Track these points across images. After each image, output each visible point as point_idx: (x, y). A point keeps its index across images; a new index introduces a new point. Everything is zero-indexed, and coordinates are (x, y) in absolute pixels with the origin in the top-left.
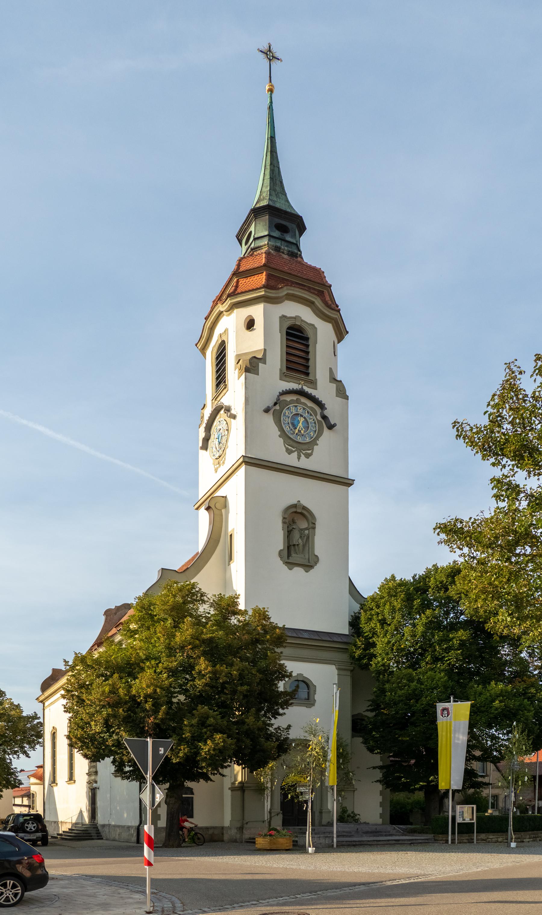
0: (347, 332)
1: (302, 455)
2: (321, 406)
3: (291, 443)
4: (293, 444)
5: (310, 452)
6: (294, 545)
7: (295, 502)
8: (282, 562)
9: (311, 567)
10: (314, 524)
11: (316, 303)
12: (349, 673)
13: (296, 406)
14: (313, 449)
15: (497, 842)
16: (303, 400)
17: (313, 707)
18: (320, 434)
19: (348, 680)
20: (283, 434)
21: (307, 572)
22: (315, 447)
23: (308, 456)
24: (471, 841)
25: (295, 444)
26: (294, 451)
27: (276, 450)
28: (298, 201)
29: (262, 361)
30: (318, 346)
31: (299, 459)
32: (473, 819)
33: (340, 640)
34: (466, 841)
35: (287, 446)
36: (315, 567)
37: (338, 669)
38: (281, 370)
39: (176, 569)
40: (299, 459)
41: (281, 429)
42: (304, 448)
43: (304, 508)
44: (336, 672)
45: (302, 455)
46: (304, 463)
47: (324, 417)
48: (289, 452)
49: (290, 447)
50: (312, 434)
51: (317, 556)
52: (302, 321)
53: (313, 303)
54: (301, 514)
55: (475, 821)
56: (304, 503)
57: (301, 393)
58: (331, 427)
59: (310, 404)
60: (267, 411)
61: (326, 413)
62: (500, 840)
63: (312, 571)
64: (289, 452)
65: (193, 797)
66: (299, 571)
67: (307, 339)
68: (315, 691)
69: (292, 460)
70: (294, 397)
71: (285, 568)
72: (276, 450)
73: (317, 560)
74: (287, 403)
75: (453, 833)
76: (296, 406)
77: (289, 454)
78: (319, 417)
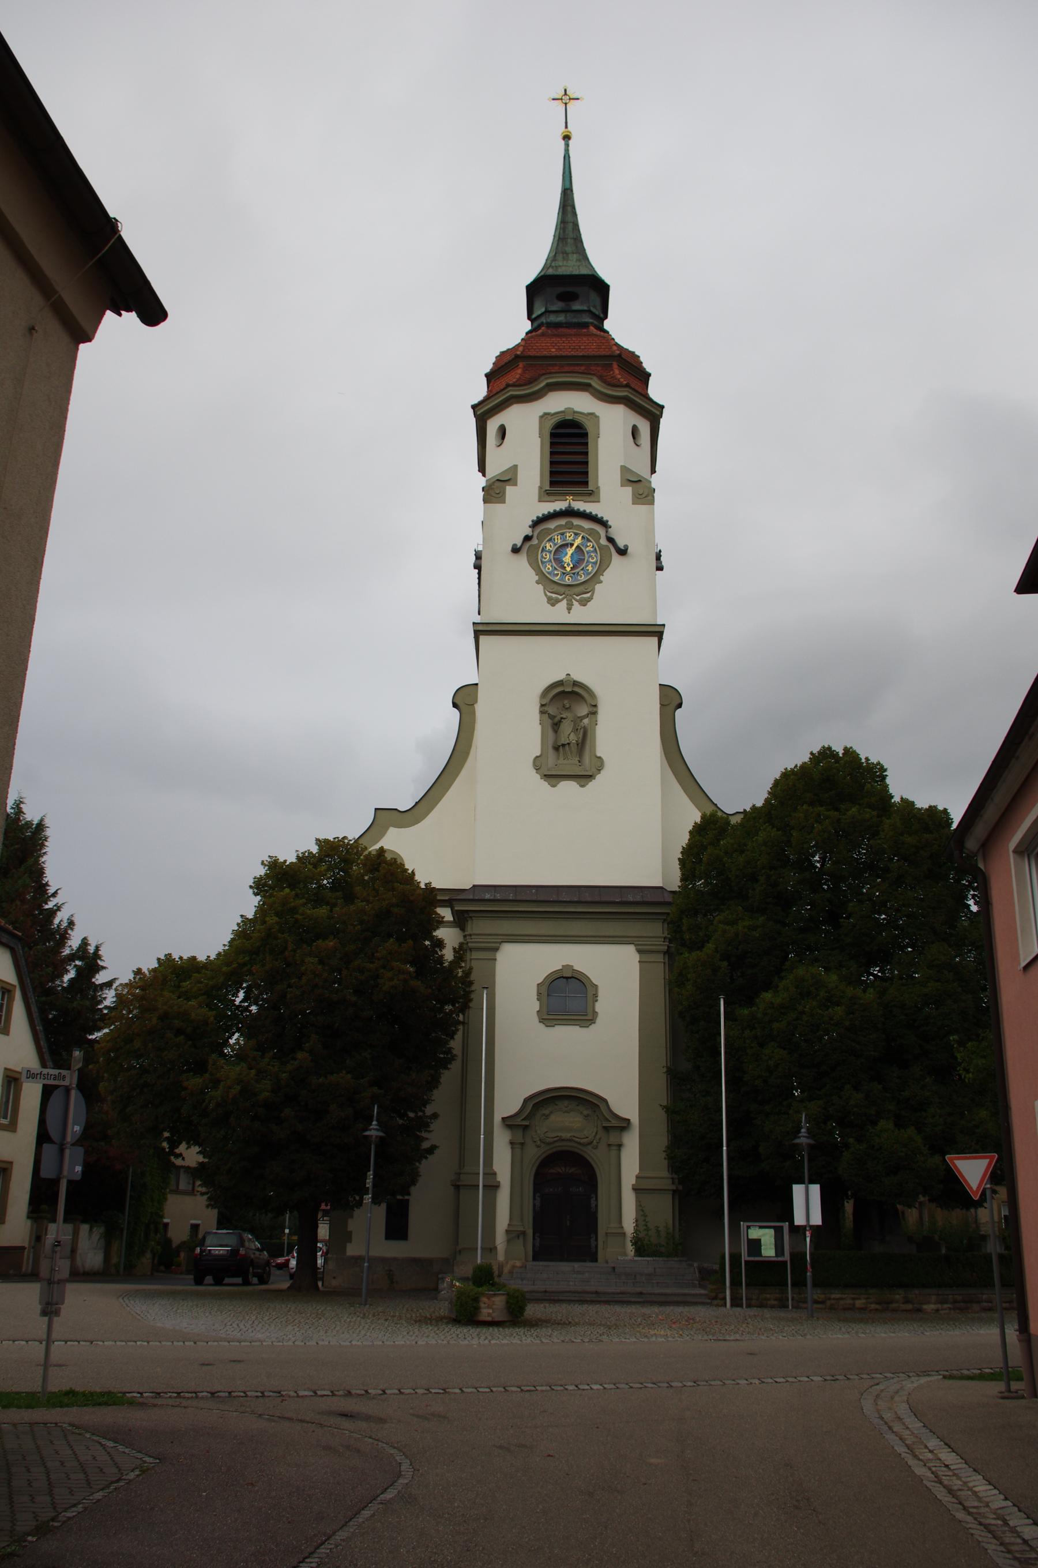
0: (662, 407)
1: (575, 602)
2: (604, 524)
3: (556, 588)
4: (559, 590)
5: (588, 595)
6: (563, 745)
7: (561, 676)
8: (538, 776)
9: (590, 777)
10: (595, 706)
11: (594, 384)
12: (660, 958)
13: (562, 534)
14: (593, 591)
15: (851, 1308)
16: (576, 522)
17: (593, 1027)
18: (603, 566)
19: (659, 971)
20: (544, 579)
21: (582, 786)
22: (597, 587)
23: (584, 603)
24: (783, 1305)
25: (562, 590)
26: (562, 600)
27: (531, 603)
28: (603, 258)
29: (511, 482)
30: (601, 442)
31: (569, 609)
32: (783, 1254)
33: (638, 898)
34: (773, 1302)
35: (549, 594)
36: (598, 777)
37: (639, 951)
38: (540, 488)
39: (403, 808)
40: (569, 609)
41: (539, 572)
42: (580, 590)
43: (576, 684)
44: (637, 957)
45: (575, 602)
46: (580, 615)
47: (611, 540)
48: (553, 602)
49: (554, 596)
50: (590, 568)
51: (600, 758)
52: (575, 412)
53: (589, 385)
54: (573, 693)
55: (787, 1257)
56: (577, 677)
57: (570, 513)
58: (623, 552)
59: (587, 525)
60: (516, 550)
61: (613, 533)
62: (859, 1303)
63: (592, 785)
64: (553, 602)
65: (408, 1200)
66: (569, 787)
67: (585, 435)
68: (596, 995)
69: (559, 614)
70: (562, 522)
71: (544, 785)
72: (531, 603)
73: (599, 764)
74: (549, 531)
75: (736, 1283)
76: (562, 534)
77: (553, 605)
78: (603, 541)
